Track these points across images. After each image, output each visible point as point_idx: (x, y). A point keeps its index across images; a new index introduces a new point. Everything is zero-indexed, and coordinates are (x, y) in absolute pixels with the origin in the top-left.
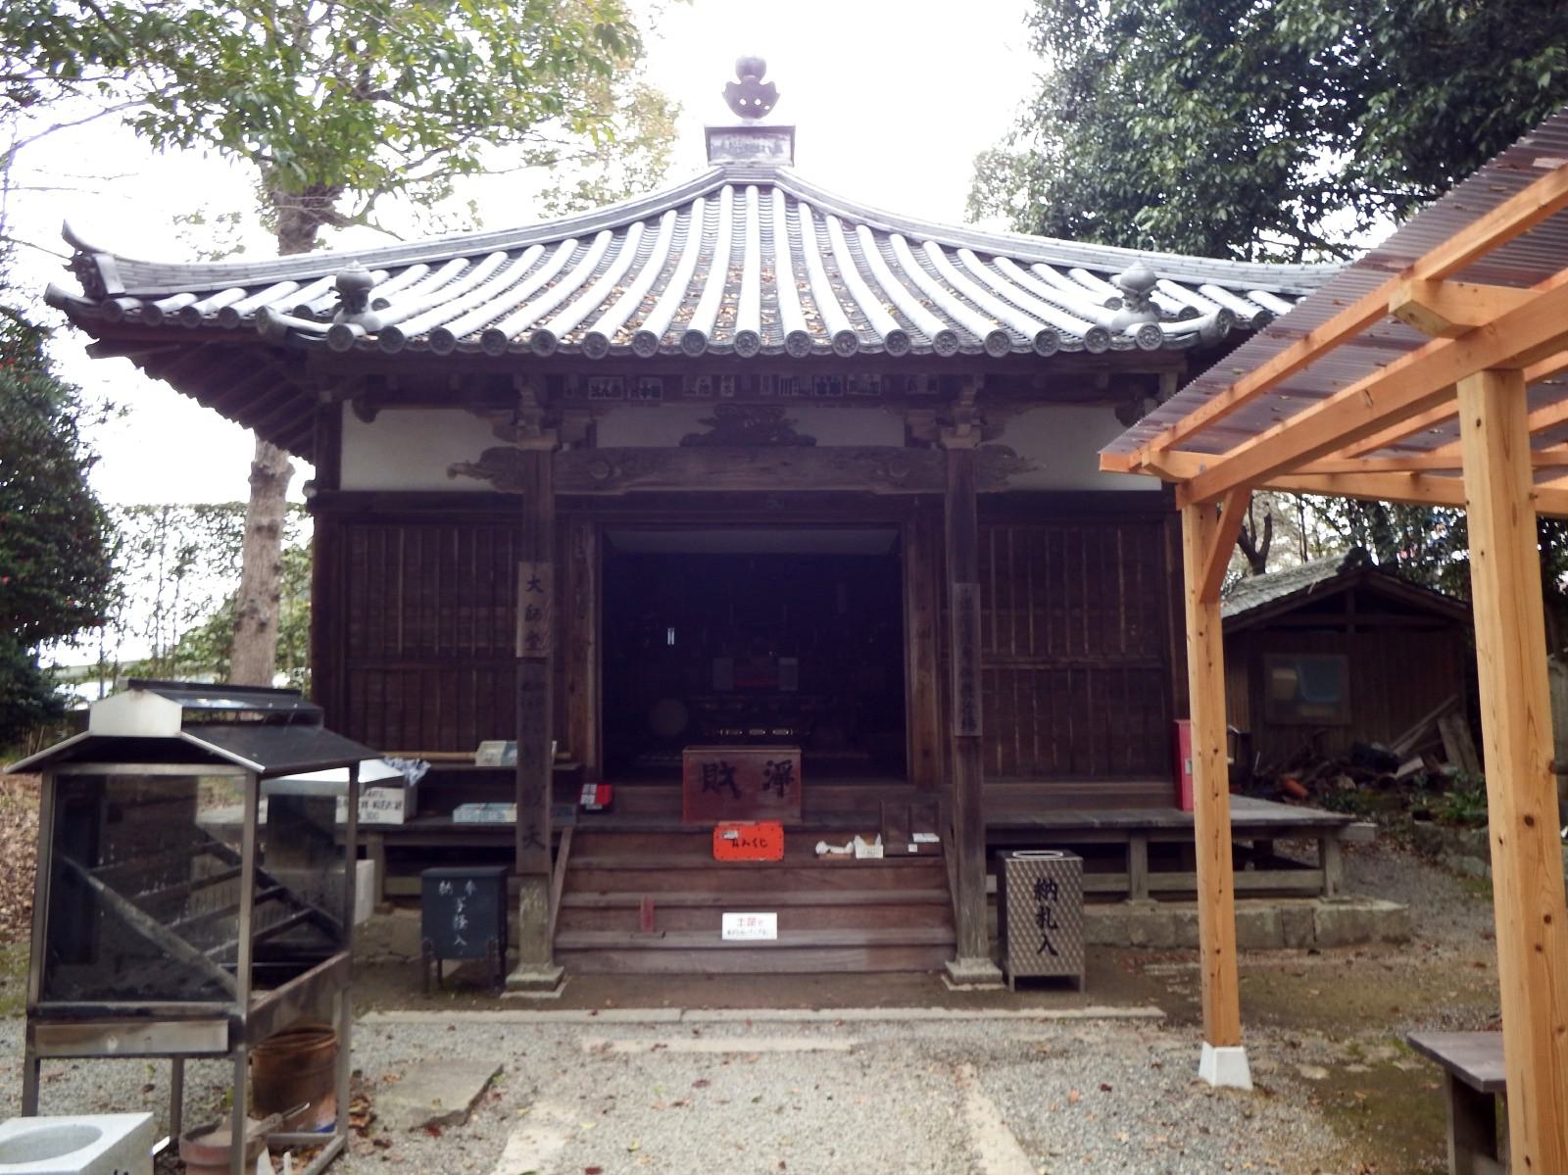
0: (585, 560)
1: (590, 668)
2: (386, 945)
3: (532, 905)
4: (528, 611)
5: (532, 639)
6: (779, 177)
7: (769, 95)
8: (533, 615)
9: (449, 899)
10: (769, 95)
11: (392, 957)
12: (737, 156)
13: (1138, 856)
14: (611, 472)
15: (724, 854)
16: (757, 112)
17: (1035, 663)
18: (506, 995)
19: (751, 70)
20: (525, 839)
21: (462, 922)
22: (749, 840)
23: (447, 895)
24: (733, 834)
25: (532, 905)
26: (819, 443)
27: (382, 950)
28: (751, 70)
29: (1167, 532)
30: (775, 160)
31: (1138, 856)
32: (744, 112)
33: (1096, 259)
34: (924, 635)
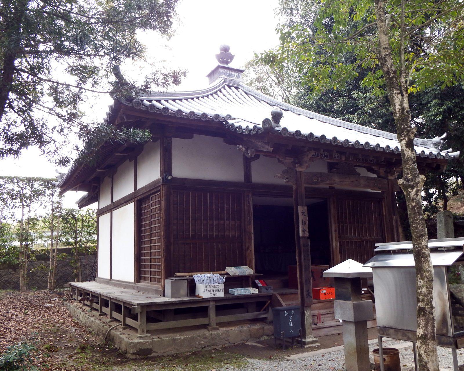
0: (250, 205)
1: (253, 241)
2: (228, 340)
3: (308, 316)
4: (302, 222)
5: (304, 230)
6: (240, 85)
7: (231, 57)
8: (303, 223)
9: (287, 317)
10: (231, 57)
11: (230, 344)
12: (227, 76)
13: (212, 312)
14: (318, 180)
15: (322, 298)
16: (227, 63)
17: (357, 239)
18: (306, 346)
19: (225, 50)
20: (306, 295)
21: (291, 324)
22: (328, 293)
23: (287, 316)
24: (324, 291)
25: (308, 316)
26: (361, 175)
27: (226, 342)
28: (225, 50)
29: (383, 204)
30: (238, 80)
31: (212, 312)
32: (221, 62)
33: (358, 128)
34: (336, 231)
